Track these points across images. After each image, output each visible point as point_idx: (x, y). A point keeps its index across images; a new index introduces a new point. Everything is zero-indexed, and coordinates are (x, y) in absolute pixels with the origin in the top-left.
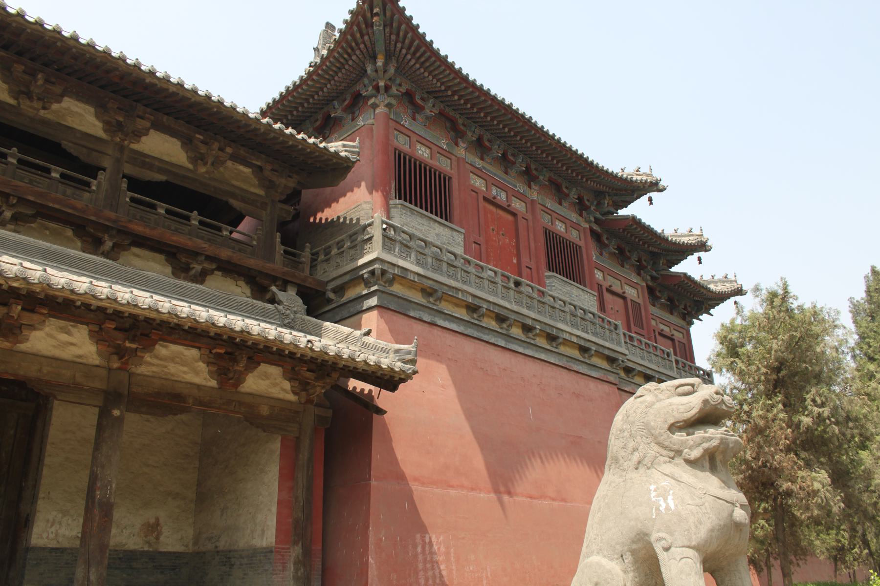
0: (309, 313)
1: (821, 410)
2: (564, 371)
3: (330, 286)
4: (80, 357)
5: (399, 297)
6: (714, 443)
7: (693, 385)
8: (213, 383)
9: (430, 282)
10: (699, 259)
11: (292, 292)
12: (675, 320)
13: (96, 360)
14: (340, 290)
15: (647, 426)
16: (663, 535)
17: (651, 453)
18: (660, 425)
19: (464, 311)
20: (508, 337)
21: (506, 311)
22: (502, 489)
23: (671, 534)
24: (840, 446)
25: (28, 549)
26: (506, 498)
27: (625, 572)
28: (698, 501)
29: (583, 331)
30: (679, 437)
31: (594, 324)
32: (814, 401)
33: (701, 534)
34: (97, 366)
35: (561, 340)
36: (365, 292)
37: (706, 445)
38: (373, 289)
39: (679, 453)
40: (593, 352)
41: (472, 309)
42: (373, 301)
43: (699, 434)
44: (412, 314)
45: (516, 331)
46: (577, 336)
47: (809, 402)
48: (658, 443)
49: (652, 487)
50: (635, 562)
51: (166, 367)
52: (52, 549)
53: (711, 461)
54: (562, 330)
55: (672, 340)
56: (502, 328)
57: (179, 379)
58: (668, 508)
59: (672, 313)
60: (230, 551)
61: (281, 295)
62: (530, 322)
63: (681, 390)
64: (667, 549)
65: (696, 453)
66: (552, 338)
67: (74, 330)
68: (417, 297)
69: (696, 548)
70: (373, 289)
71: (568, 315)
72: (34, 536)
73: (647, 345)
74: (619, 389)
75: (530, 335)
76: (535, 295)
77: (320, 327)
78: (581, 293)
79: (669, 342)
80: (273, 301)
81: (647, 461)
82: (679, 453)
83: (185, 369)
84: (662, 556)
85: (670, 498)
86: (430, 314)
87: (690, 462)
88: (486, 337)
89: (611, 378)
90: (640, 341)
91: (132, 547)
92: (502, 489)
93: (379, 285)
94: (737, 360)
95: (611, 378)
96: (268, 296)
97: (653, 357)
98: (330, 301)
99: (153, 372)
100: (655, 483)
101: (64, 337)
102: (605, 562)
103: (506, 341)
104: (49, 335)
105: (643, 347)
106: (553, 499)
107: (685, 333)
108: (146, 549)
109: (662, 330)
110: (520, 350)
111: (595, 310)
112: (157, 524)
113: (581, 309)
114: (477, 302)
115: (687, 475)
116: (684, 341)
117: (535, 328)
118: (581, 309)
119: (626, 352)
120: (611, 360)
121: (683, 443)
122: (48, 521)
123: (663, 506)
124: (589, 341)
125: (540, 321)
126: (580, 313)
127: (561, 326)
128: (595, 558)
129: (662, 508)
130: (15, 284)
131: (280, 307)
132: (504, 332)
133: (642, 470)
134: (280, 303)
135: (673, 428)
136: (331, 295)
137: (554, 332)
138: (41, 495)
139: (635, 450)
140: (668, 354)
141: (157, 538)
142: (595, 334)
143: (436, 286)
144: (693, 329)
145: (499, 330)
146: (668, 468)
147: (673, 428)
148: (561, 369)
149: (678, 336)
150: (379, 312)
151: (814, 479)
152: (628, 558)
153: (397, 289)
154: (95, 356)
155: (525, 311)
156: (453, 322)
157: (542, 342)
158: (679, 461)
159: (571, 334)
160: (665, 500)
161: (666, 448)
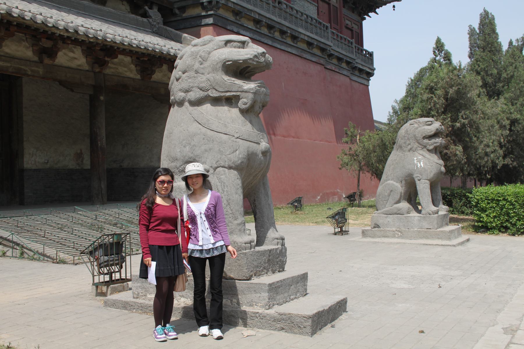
0: (165, 23)
1: (464, 121)
2: (299, 58)
3: (176, 6)
4: (79, 66)
5: (223, 18)
6: (438, 144)
7: (432, 122)
8: (139, 77)
9: (239, 7)
10: (394, 7)
11: (155, 10)
12: (355, 17)
13: (86, 67)
14: (183, 9)
15: (415, 136)
16: (419, 175)
17: (415, 146)
18: (419, 136)
19: (252, 23)
20: (273, 39)
21: (274, 22)
22: (271, 132)
23: (422, 175)
24: (426, 89)
25: (22, 170)
26: (273, 137)
27: (402, 187)
28: (431, 164)
29: (311, 32)
30: (426, 141)
31: (316, 27)
32: (462, 116)
33: (431, 175)
34: (87, 71)
35: (300, 39)
36: (204, 14)
37: (435, 145)
38: (210, 13)
39: (425, 147)
40: (315, 46)
41: (257, 22)
42: (210, 21)
43: (433, 141)
44: (229, 28)
45: (277, 35)
46: (308, 36)
47: (460, 117)
48: (419, 143)
49: (415, 158)
50: (406, 184)
51: (117, 69)
52: (35, 170)
53: (436, 150)
54: (301, 33)
55: (352, 30)
56: (270, 33)
57: (123, 75)
58: (421, 166)
59: (353, 12)
60: (133, 169)
61: (151, 12)
62: (285, 29)
63: (427, 123)
64: (419, 180)
65: (431, 147)
66: (294, 38)
67: (75, 50)
68: (231, 17)
69: (429, 180)
70: (210, 13)
71: (304, 22)
72: (25, 163)
73: (341, 38)
74: (325, 68)
75: (284, 36)
76: (288, 10)
77: (181, 37)
78: (309, 5)
79: (350, 32)
80: (145, 15)
81: (414, 149)
82: (425, 147)
83: (126, 69)
84: (417, 182)
85: (422, 163)
86: (237, 27)
87: (428, 150)
88: (263, 40)
89: (322, 61)
90: (337, 35)
91: (71, 167)
92: (271, 132)
93: (214, 11)
94: (433, 95)
95: (322, 61)
96: (141, 12)
97: (344, 46)
98: (175, 15)
99: (112, 72)
100: (416, 157)
101: (71, 55)
102: (395, 183)
103: (272, 41)
104: (65, 54)
105: (339, 39)
106: (294, 137)
107: (359, 24)
108: (78, 168)
109: (347, 25)
110: (279, 46)
111: (315, 16)
112: (81, 153)
113: (305, 14)
114: (260, 18)
115: (427, 155)
116: (358, 31)
117: (288, 32)
118: (305, 14)
119: (332, 44)
120: (323, 50)
121: (427, 143)
122: (30, 154)
123: (419, 165)
124: (314, 39)
125: (290, 28)
126: (309, 20)
127: (300, 30)
128: (390, 182)
129: (419, 166)
130: (92, 40)
131: (151, 20)
132: (272, 36)
133: (411, 152)
134: (150, 17)
135: (424, 138)
136: (177, 11)
137: (297, 34)
138: (25, 139)
139: (409, 144)
140: (352, 43)
141: (82, 161)
142: (316, 34)
143: (241, 10)
144: (364, 22)
145: (269, 35)
146: (421, 152)
147: (424, 138)
148: (298, 57)
149: (355, 27)
150: (214, 28)
151: (457, 150)
152: (404, 182)
153: (221, 12)
154: (86, 65)
155: (283, 22)
156: (248, 31)
157: (289, 41)
158: (425, 149)
159: (305, 35)
160: (420, 163)
161: (421, 145)
